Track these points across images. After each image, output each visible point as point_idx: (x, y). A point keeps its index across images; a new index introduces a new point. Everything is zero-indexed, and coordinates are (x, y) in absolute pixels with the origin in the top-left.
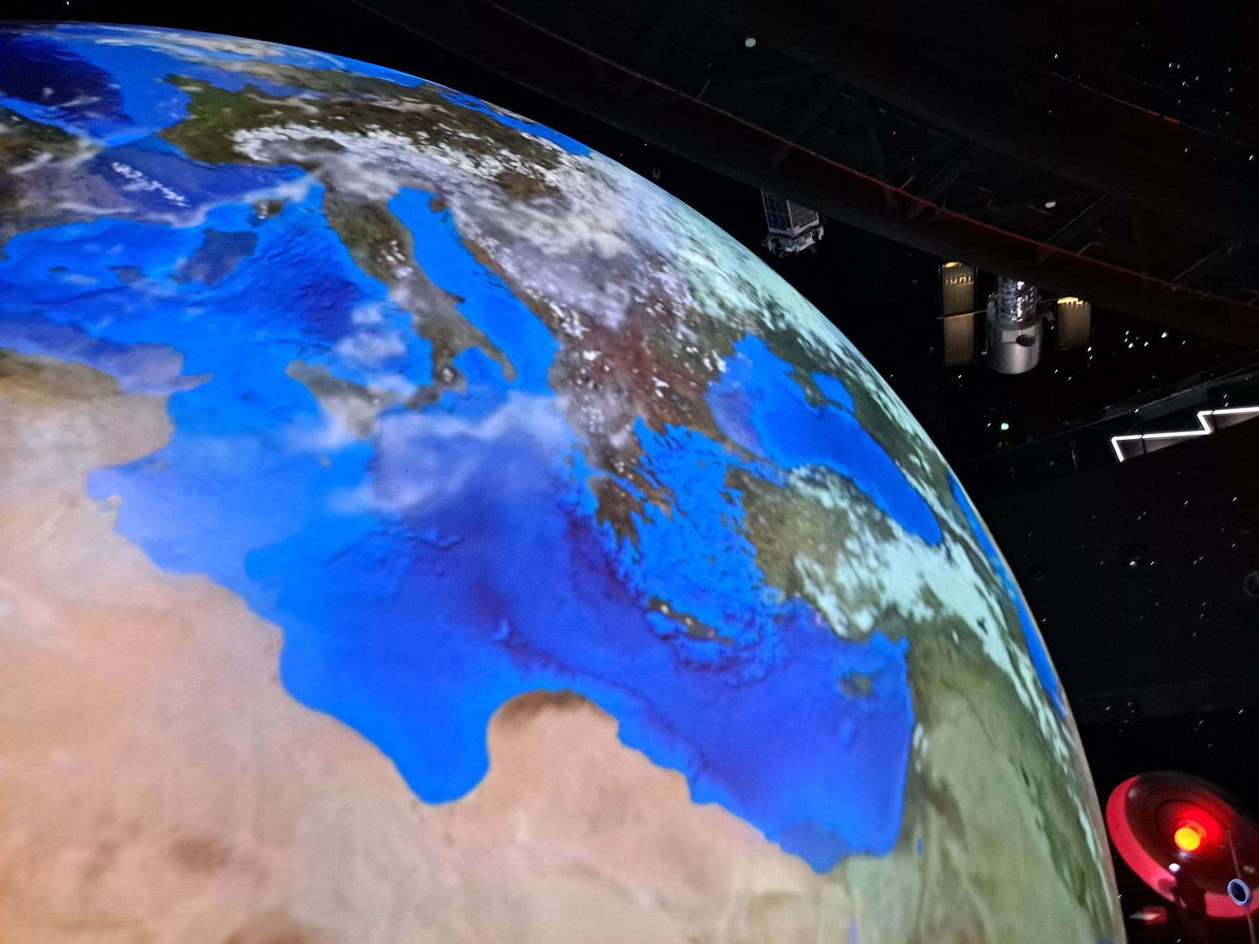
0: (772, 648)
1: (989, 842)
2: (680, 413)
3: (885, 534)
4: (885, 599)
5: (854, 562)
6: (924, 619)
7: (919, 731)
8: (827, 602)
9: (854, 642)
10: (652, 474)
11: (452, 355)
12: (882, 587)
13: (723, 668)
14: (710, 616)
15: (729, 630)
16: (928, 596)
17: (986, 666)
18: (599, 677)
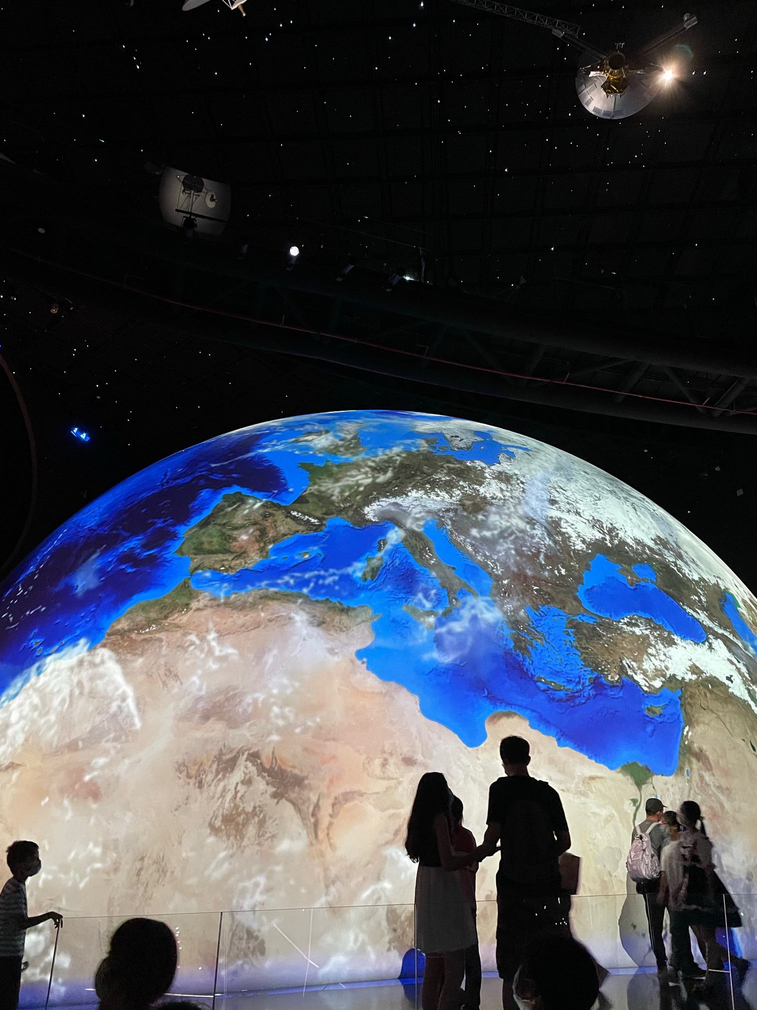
0: (589, 691)
1: (726, 773)
2: (545, 599)
3: (672, 643)
4: (668, 673)
5: (652, 658)
6: (691, 680)
7: (687, 729)
8: (639, 678)
9: (654, 695)
10: (533, 628)
11: (454, 593)
12: (667, 668)
13: (567, 700)
14: (560, 682)
15: (571, 687)
16: (695, 669)
17: (731, 698)
18: (520, 706)
